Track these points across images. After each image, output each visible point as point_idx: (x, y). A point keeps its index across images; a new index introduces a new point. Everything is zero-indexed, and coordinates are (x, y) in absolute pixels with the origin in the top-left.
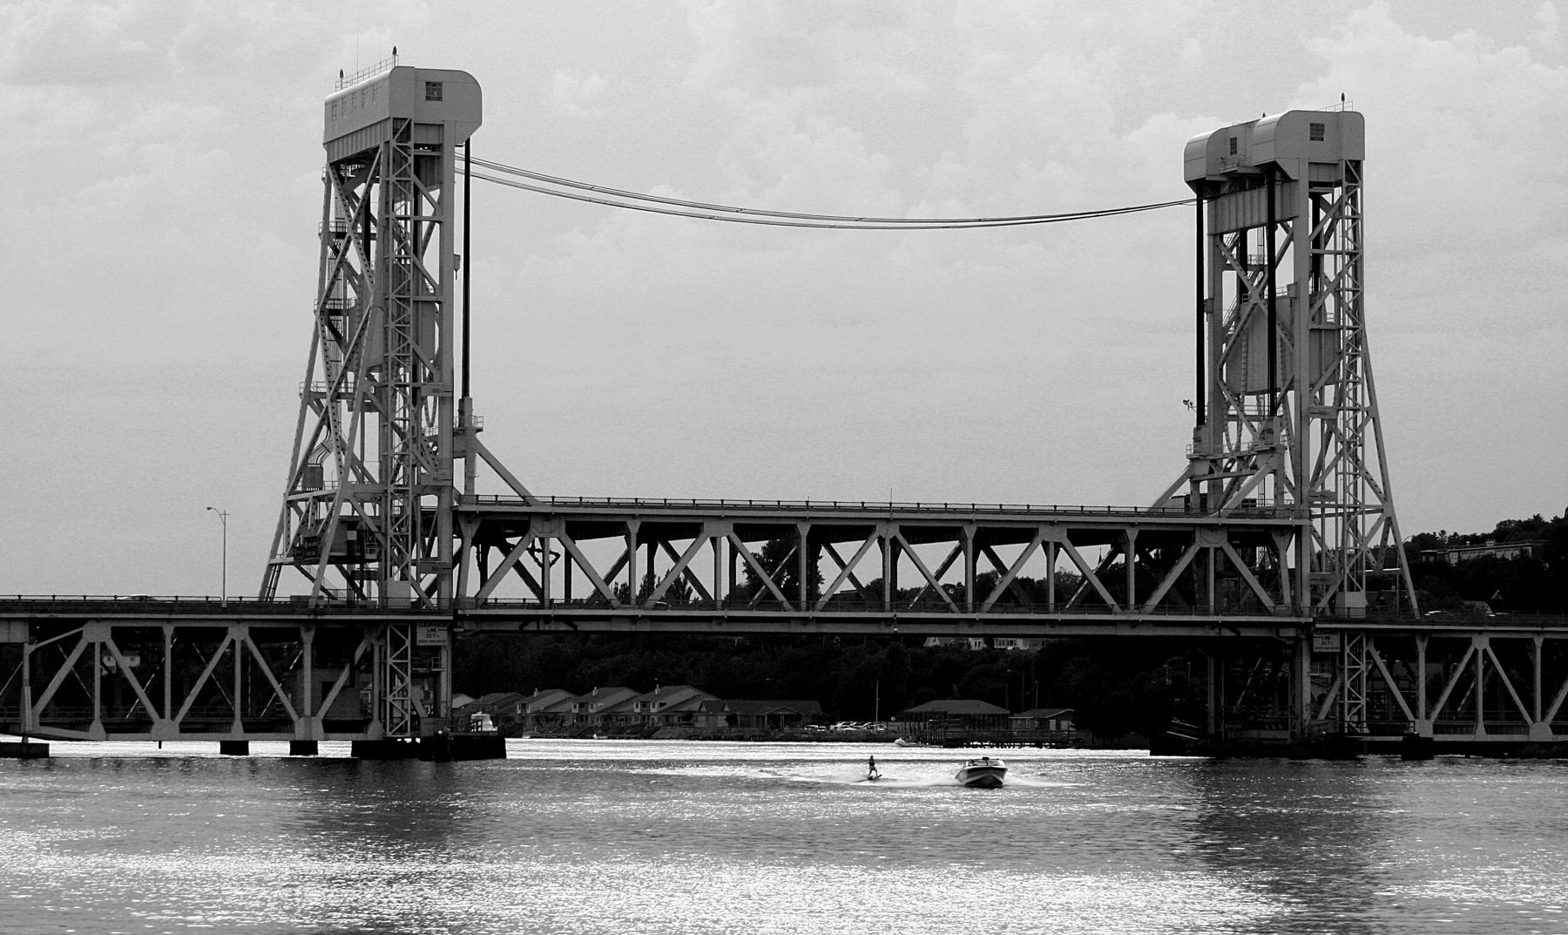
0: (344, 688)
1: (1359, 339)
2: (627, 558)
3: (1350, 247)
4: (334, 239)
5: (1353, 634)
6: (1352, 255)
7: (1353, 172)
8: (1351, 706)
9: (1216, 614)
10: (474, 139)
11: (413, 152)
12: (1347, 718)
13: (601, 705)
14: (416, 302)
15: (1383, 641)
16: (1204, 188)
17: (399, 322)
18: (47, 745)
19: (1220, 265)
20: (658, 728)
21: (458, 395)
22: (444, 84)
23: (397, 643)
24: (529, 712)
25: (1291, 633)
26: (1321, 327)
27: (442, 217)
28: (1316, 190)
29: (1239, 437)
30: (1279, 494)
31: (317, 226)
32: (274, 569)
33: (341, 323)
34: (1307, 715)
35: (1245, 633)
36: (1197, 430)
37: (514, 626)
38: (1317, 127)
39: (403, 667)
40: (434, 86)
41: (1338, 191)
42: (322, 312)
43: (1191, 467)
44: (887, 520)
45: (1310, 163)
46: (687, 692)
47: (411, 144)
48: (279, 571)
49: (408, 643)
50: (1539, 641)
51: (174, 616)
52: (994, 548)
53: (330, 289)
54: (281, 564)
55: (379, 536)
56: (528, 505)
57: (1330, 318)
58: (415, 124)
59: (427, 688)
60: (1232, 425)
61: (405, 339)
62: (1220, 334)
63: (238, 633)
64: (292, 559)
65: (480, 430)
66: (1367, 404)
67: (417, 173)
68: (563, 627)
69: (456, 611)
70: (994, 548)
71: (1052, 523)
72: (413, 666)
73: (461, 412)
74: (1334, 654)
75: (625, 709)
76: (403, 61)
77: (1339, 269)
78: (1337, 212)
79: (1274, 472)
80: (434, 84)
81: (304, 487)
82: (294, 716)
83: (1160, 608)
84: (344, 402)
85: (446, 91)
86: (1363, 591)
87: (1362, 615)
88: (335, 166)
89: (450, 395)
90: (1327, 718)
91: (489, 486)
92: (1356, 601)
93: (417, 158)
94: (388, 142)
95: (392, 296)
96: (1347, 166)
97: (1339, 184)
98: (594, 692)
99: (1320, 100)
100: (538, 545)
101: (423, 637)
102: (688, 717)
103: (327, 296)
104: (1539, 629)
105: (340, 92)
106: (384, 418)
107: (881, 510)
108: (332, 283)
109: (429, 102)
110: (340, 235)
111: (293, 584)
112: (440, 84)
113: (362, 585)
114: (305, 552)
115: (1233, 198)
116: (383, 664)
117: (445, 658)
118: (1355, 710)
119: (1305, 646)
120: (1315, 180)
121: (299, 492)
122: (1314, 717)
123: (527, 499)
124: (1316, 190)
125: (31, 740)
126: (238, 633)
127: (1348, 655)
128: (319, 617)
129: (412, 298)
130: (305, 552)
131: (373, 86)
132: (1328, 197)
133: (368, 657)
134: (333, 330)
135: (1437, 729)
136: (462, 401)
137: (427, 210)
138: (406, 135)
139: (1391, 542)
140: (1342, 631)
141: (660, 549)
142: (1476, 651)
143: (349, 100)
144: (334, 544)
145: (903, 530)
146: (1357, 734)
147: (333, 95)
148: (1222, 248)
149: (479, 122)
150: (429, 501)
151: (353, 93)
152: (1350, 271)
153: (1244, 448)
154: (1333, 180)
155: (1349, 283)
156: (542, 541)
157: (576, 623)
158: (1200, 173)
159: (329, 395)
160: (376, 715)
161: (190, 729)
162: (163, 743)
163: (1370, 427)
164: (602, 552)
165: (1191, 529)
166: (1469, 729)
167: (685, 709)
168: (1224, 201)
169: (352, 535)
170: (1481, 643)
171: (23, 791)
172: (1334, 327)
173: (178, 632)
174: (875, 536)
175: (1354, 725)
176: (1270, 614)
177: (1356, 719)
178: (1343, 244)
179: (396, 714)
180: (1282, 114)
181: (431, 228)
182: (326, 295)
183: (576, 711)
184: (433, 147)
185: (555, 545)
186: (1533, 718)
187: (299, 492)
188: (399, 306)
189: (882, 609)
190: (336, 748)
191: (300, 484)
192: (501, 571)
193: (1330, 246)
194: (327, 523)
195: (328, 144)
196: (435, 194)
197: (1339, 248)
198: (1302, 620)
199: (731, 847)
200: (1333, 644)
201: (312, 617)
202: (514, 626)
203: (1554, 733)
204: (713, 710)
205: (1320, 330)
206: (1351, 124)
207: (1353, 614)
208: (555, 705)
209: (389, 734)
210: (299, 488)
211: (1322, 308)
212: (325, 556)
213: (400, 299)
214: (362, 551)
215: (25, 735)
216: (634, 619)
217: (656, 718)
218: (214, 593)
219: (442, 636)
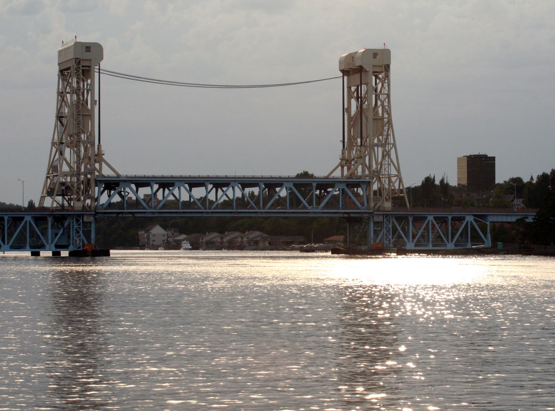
0: (61, 235)
1: (390, 122)
3: (387, 92)
4: (61, 94)
5: (387, 216)
6: (387, 95)
7: (387, 68)
8: (386, 238)
9: (342, 209)
10: (101, 63)
12: (385, 242)
13: (228, 238)
14: (83, 115)
15: (399, 219)
16: (345, 72)
17: (78, 122)
19: (350, 97)
20: (246, 246)
22: (91, 47)
23: (78, 221)
24: (204, 241)
25: (367, 215)
26: (377, 118)
28: (375, 74)
30: (363, 171)
31: (56, 91)
32: (43, 198)
34: (372, 242)
35: (352, 215)
36: (343, 150)
37: (115, 215)
38: (375, 54)
39: (80, 228)
40: (88, 47)
43: (341, 162)
44: (234, 181)
45: (373, 66)
46: (258, 233)
47: (81, 66)
48: (44, 199)
49: (81, 221)
50: (450, 217)
51: (7, 213)
54: (45, 196)
55: (72, 188)
56: (119, 178)
58: (82, 60)
59: (173, 232)
61: (79, 127)
62: (350, 119)
63: (28, 218)
65: (103, 154)
66: (392, 142)
67: (83, 75)
68: (130, 215)
71: (288, 181)
72: (82, 228)
73: (98, 149)
74: (382, 222)
75: (235, 240)
76: (79, 40)
79: (361, 164)
81: (52, 172)
82: (46, 244)
83: (324, 208)
85: (92, 49)
86: (390, 202)
87: (390, 209)
89: (93, 144)
90: (379, 242)
91: (106, 172)
92: (388, 205)
93: (83, 70)
94: (73, 66)
95: (75, 113)
96: (385, 66)
98: (226, 233)
99: (377, 45)
100: (122, 190)
101: (86, 219)
102: (256, 243)
104: (449, 213)
105: (63, 48)
107: (233, 178)
109: (87, 53)
110: (62, 93)
111: (48, 203)
112: (90, 47)
113: (71, 202)
114: (50, 193)
116: (73, 227)
117: (93, 226)
118: (387, 240)
119: (371, 219)
121: (50, 174)
122: (375, 241)
123: (118, 176)
124: (375, 74)
126: (28, 218)
127: (386, 223)
128: (53, 213)
129: (81, 113)
130: (50, 193)
131: (69, 47)
132: (380, 76)
133: (69, 225)
134: (61, 122)
135: (416, 246)
136: (98, 146)
138: (79, 63)
139: (401, 188)
140: (383, 214)
142: (26, 221)
144: (58, 190)
146: (389, 247)
147: (60, 49)
148: (351, 92)
149: (102, 59)
154: (381, 71)
156: (124, 188)
157: (134, 214)
158: (343, 68)
159: (58, 143)
160: (71, 243)
161: (14, 247)
162: (5, 252)
165: (334, 183)
166: (427, 245)
167: (256, 239)
168: (351, 76)
169: (63, 188)
170: (431, 218)
172: (381, 118)
173: (377, 195)
174: (231, 185)
175: (387, 244)
176: (360, 209)
177: (388, 242)
178: (384, 91)
179: (78, 243)
180: (347, 54)
182: (59, 110)
183: (219, 240)
184: (88, 67)
186: (448, 242)
187: (50, 174)
188: (78, 117)
189: (233, 209)
190: (65, 253)
191: (51, 171)
192: (168, 195)
194: (56, 184)
195: (59, 64)
198: (370, 211)
200: (380, 219)
201: (50, 213)
202: (115, 215)
203: (455, 246)
204: (264, 239)
205: (376, 119)
206: (386, 53)
207: (386, 209)
208: (213, 238)
211: (377, 112)
212: (55, 193)
213: (78, 114)
214: (66, 192)
216: (153, 213)
217: (246, 243)
219: (92, 219)
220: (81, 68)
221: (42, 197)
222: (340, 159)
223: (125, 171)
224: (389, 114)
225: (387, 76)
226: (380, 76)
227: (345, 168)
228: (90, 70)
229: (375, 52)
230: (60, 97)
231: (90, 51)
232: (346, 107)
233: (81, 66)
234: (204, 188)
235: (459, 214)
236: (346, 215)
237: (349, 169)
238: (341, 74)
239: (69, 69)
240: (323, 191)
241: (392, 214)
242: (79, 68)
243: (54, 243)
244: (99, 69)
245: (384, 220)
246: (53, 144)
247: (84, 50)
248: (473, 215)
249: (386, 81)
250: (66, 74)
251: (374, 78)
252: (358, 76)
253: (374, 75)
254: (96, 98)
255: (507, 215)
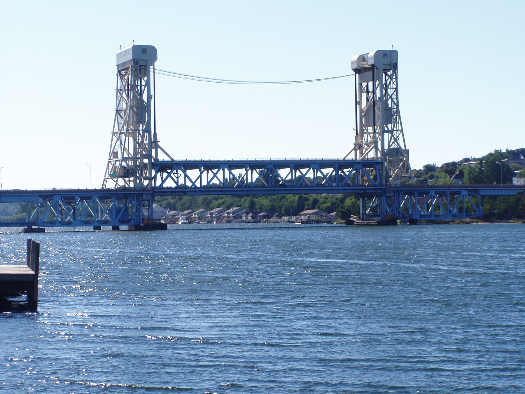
1: (398, 111)
2: (200, 176)
5: (397, 191)
10: (155, 63)
11: (139, 67)
14: (141, 108)
16: (357, 71)
18: (44, 229)
19: (361, 92)
21: (153, 132)
25: (380, 191)
27: (148, 84)
28: (385, 71)
29: (367, 138)
33: (122, 113)
35: (368, 191)
36: (356, 137)
41: (391, 71)
42: (117, 111)
45: (384, 64)
47: (138, 66)
49: (141, 199)
50: (448, 192)
52: (301, 170)
53: (119, 105)
57: (390, 106)
60: (365, 135)
62: (361, 111)
64: (110, 177)
66: (400, 129)
69: (153, 190)
70: (301, 170)
76: (136, 43)
77: (392, 93)
78: (391, 77)
80: (145, 49)
84: (123, 134)
88: (119, 72)
91: (162, 157)
97: (391, 70)
100: (175, 172)
103: (118, 106)
106: (135, 140)
108: (119, 103)
110: (121, 90)
111: (111, 185)
115: (364, 73)
120: (385, 69)
124: (385, 71)
125: (40, 227)
132: (389, 73)
137: (144, 83)
141: (210, 171)
143: (122, 53)
145: (274, 166)
150: (146, 161)
151: (123, 52)
152: (395, 93)
153: (369, 142)
155: (395, 96)
158: (355, 67)
162: (76, 227)
163: (401, 135)
164: (193, 174)
169: (126, 171)
171: (454, 265)
177: (398, 214)
181: (145, 88)
182: (118, 105)
185: (180, 172)
193: (390, 87)
195: (118, 66)
196: (145, 79)
197: (392, 87)
198: (383, 188)
199: (458, 265)
203: (435, 217)
209: (136, 224)
210: (112, 158)
215: (39, 226)
218: (89, 188)
220: (139, 67)
221: (104, 179)
222: (354, 144)
223: (179, 156)
224: (398, 106)
225: (395, 72)
226: (389, 73)
227: (358, 152)
228: (146, 69)
229: (385, 53)
230: (119, 94)
231: (146, 53)
232: (358, 100)
233: (138, 66)
234: (244, 169)
235: (260, 190)
236: (363, 191)
237: (362, 153)
238: (354, 73)
239: (127, 69)
240: (340, 172)
241: (401, 190)
242: (137, 67)
243: (118, 218)
244: (154, 69)
245: (394, 194)
246: (114, 133)
247: (141, 51)
248: (467, 190)
249: (394, 77)
250: (123, 73)
251: (384, 74)
252: (370, 73)
253: (384, 73)
254: (152, 93)
255: (487, 189)
